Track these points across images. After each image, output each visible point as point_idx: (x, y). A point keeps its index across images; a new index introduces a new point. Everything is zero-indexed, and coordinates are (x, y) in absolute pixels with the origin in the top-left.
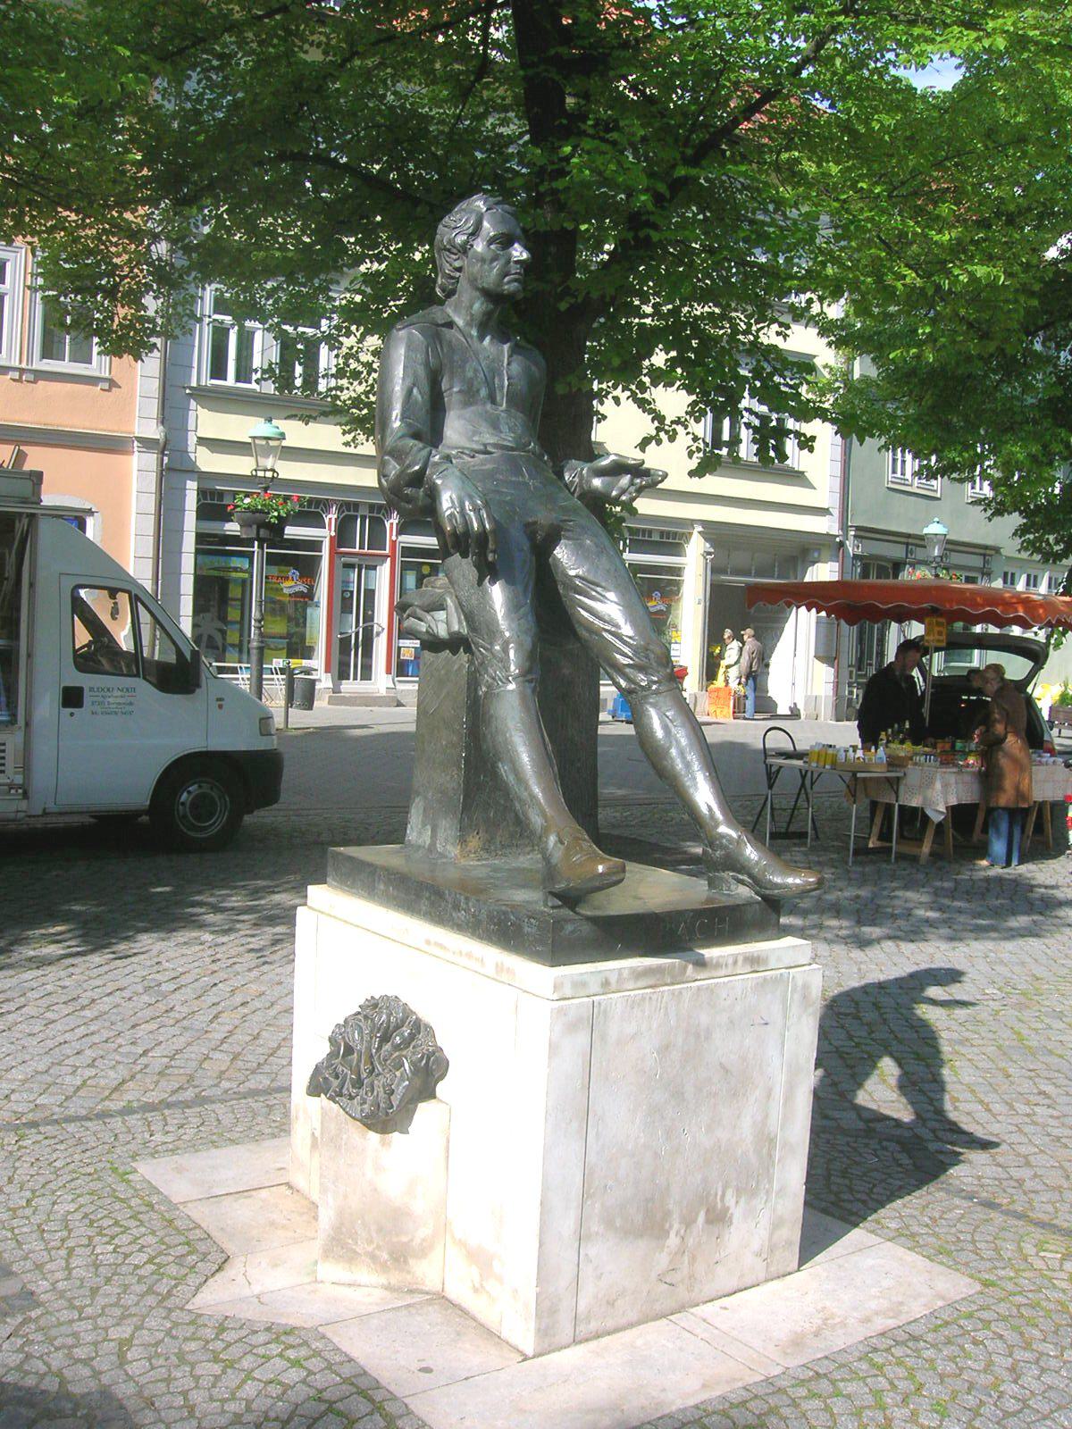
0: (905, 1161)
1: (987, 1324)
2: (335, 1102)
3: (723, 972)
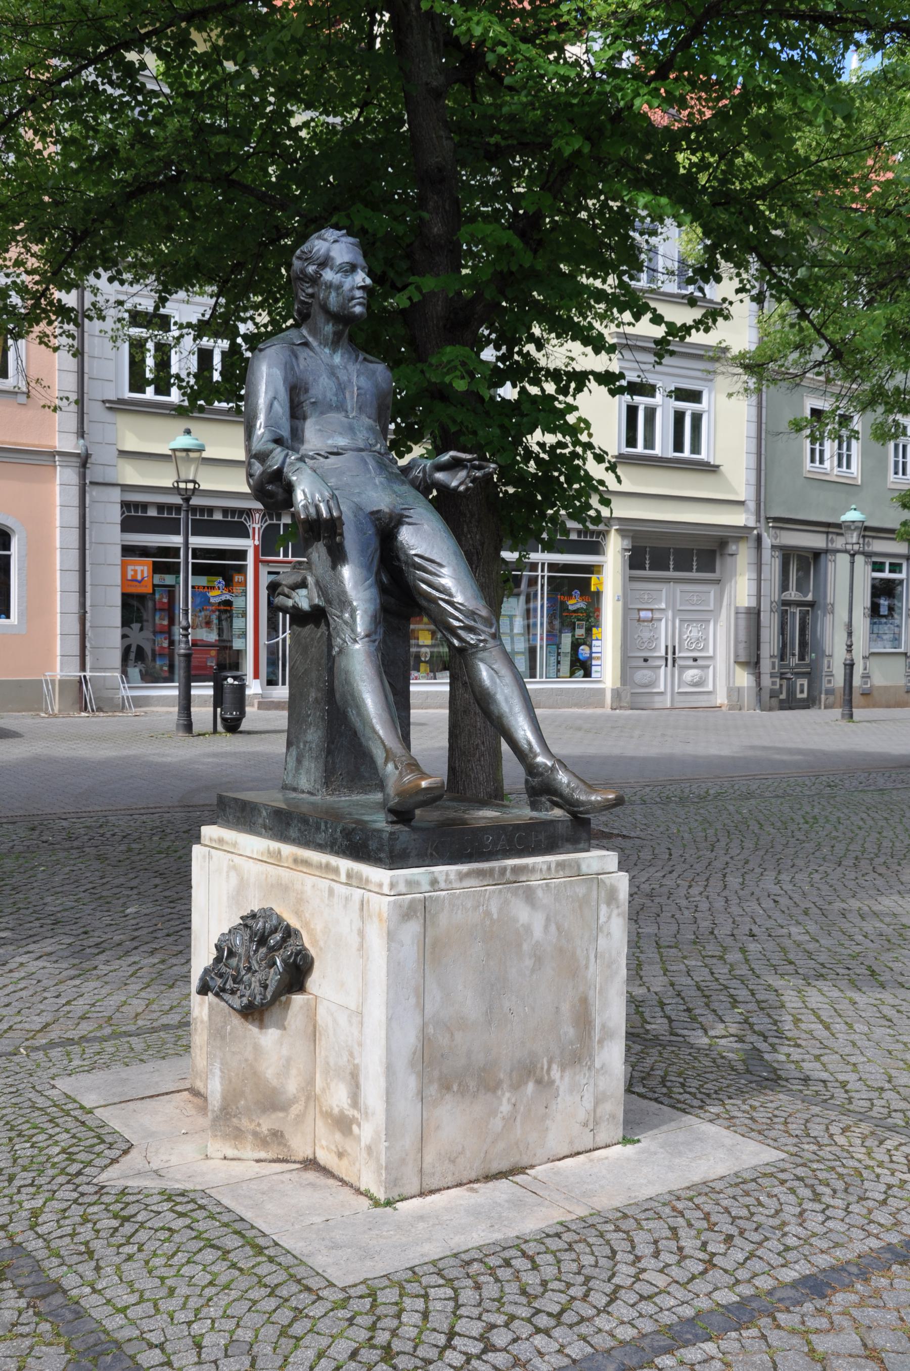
1: (783, 1182)
2: (222, 999)
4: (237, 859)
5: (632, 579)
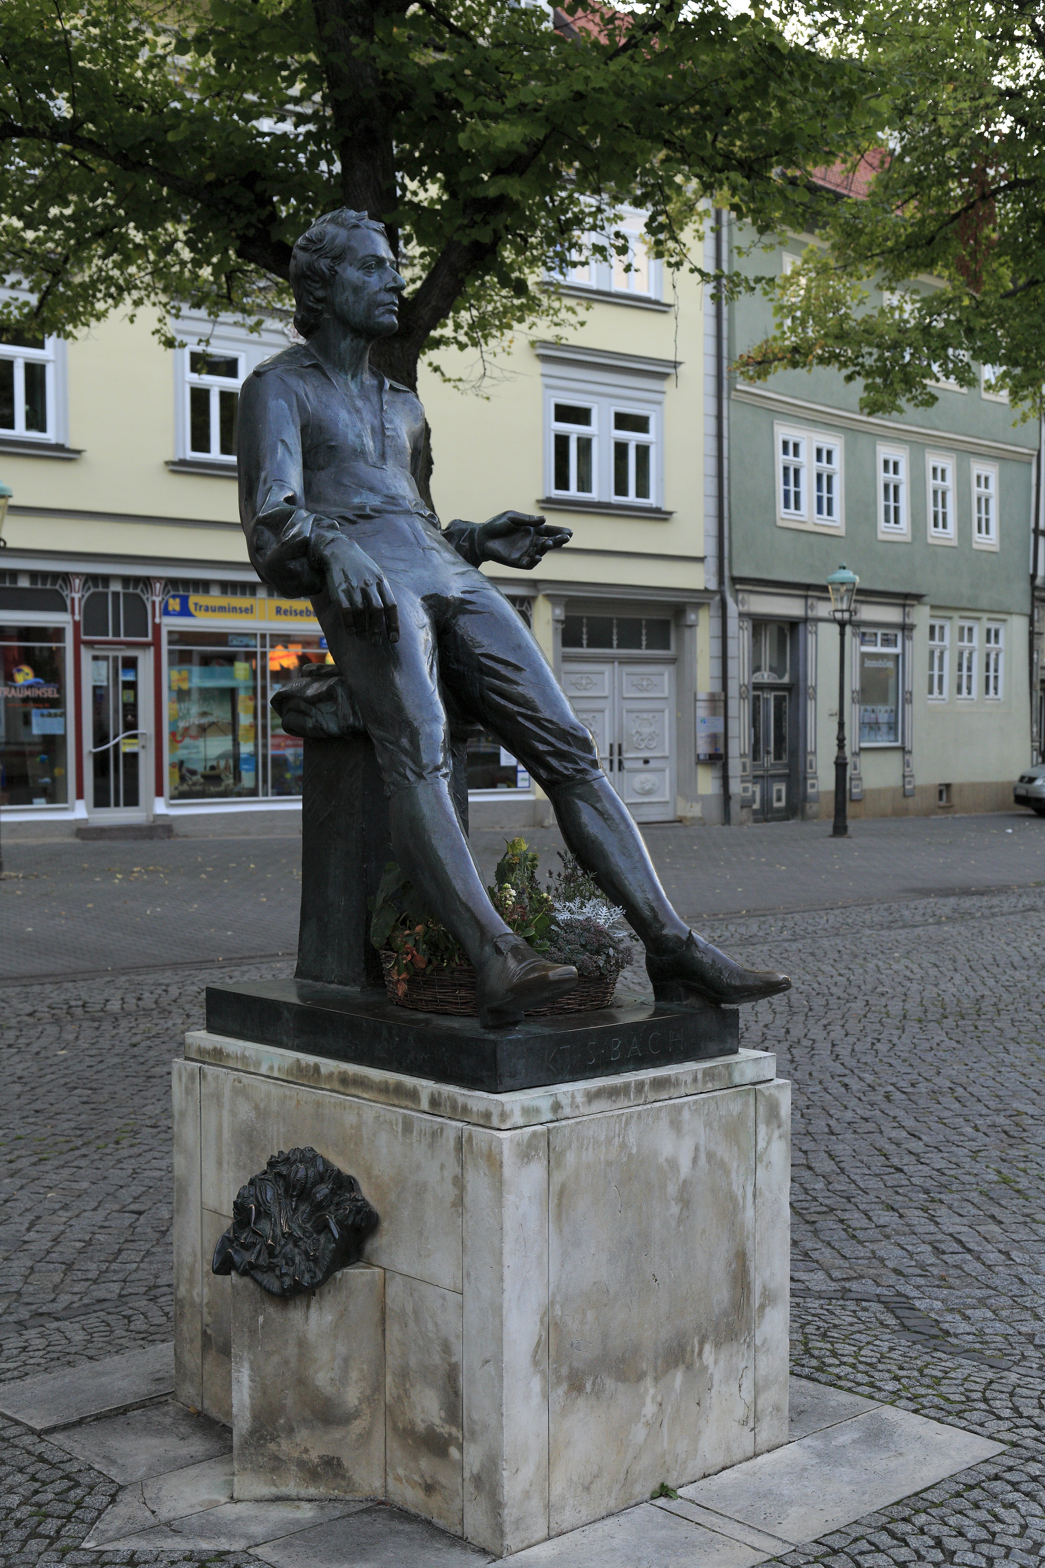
0: (891, 1321)
3: (683, 1090)
4: (247, 1079)
5: (566, 659)
